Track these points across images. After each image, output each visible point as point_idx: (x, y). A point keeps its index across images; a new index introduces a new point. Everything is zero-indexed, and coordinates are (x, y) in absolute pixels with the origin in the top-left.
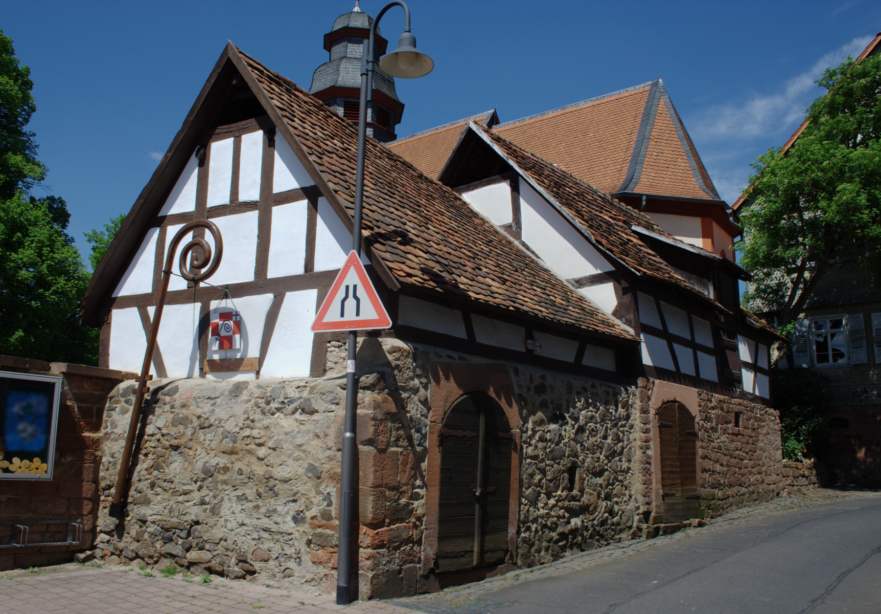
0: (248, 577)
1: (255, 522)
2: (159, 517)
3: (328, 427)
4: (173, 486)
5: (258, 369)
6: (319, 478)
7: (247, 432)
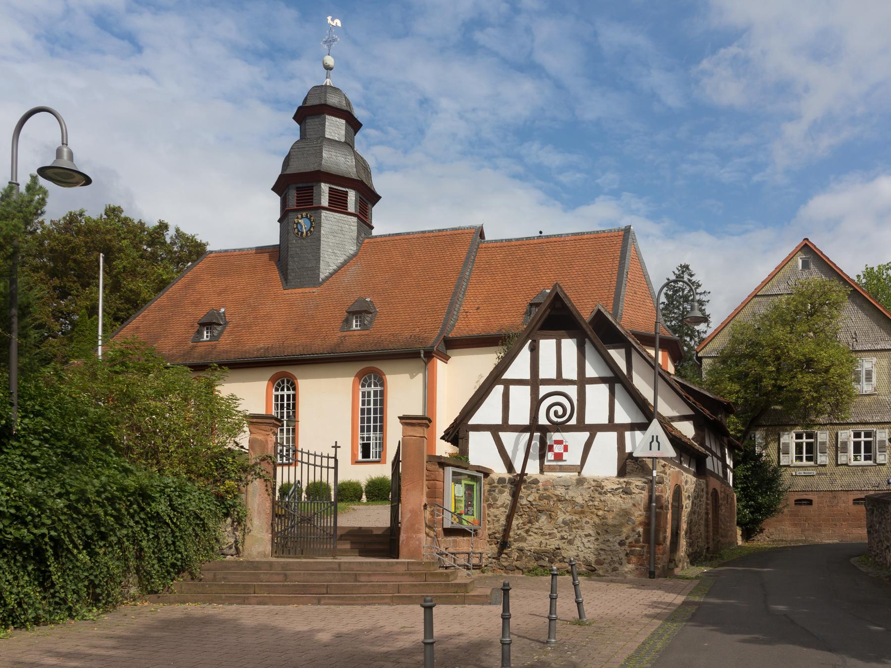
5: (579, 471)
7: (591, 503)
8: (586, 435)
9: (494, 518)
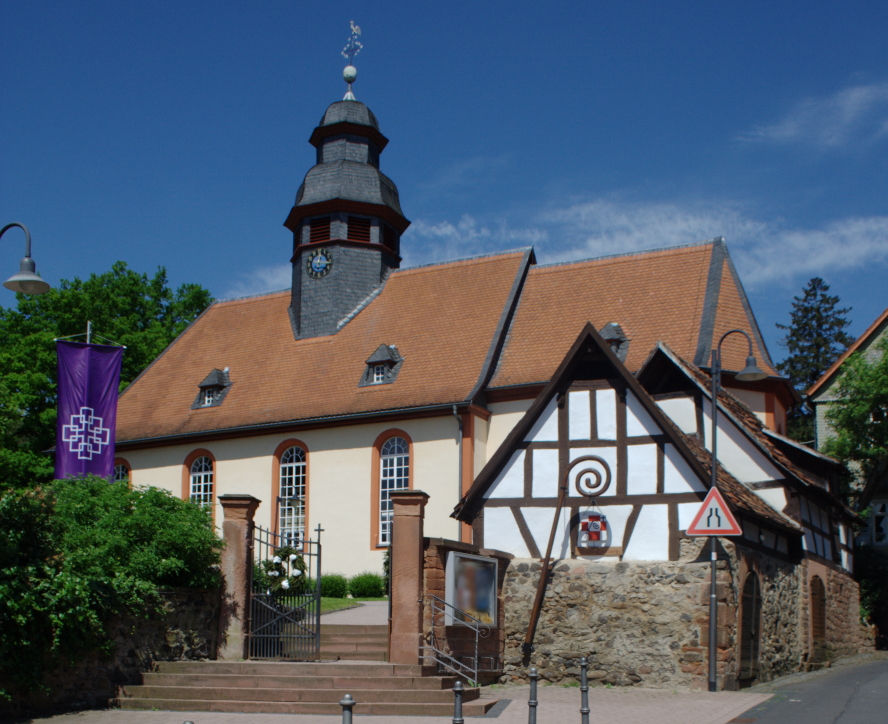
0: (636, 684)
1: (641, 650)
2: (561, 651)
3: (697, 592)
4: (573, 630)
6: (690, 621)
7: (634, 595)
8: (628, 509)
9: (514, 615)
